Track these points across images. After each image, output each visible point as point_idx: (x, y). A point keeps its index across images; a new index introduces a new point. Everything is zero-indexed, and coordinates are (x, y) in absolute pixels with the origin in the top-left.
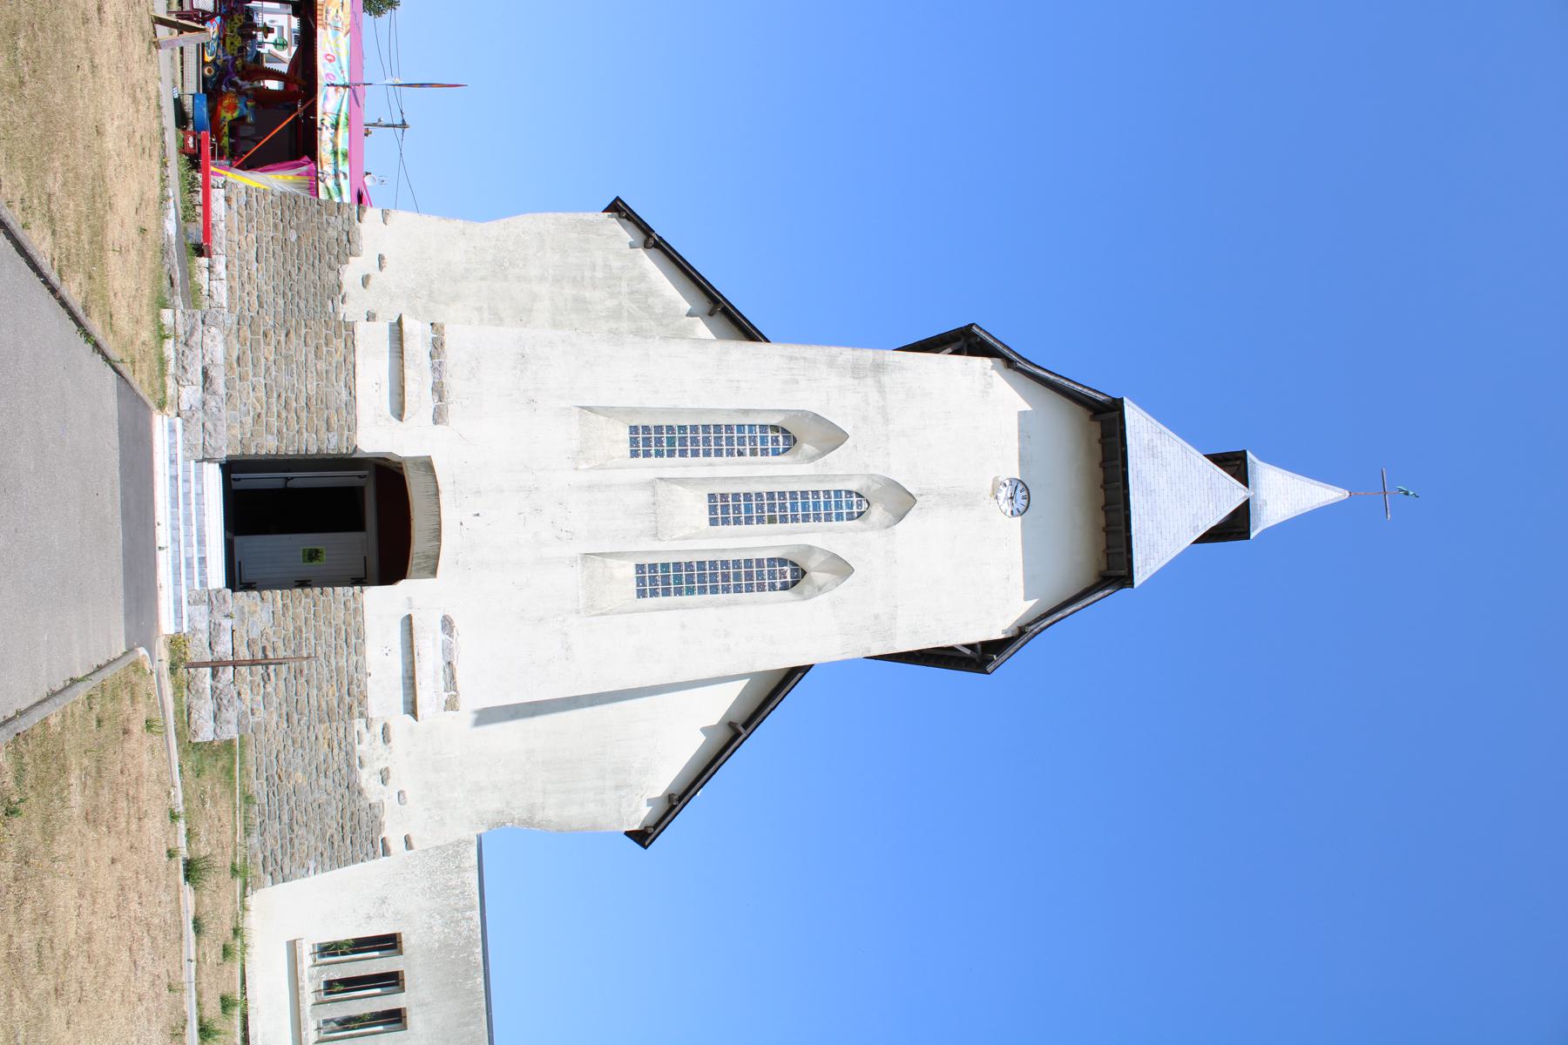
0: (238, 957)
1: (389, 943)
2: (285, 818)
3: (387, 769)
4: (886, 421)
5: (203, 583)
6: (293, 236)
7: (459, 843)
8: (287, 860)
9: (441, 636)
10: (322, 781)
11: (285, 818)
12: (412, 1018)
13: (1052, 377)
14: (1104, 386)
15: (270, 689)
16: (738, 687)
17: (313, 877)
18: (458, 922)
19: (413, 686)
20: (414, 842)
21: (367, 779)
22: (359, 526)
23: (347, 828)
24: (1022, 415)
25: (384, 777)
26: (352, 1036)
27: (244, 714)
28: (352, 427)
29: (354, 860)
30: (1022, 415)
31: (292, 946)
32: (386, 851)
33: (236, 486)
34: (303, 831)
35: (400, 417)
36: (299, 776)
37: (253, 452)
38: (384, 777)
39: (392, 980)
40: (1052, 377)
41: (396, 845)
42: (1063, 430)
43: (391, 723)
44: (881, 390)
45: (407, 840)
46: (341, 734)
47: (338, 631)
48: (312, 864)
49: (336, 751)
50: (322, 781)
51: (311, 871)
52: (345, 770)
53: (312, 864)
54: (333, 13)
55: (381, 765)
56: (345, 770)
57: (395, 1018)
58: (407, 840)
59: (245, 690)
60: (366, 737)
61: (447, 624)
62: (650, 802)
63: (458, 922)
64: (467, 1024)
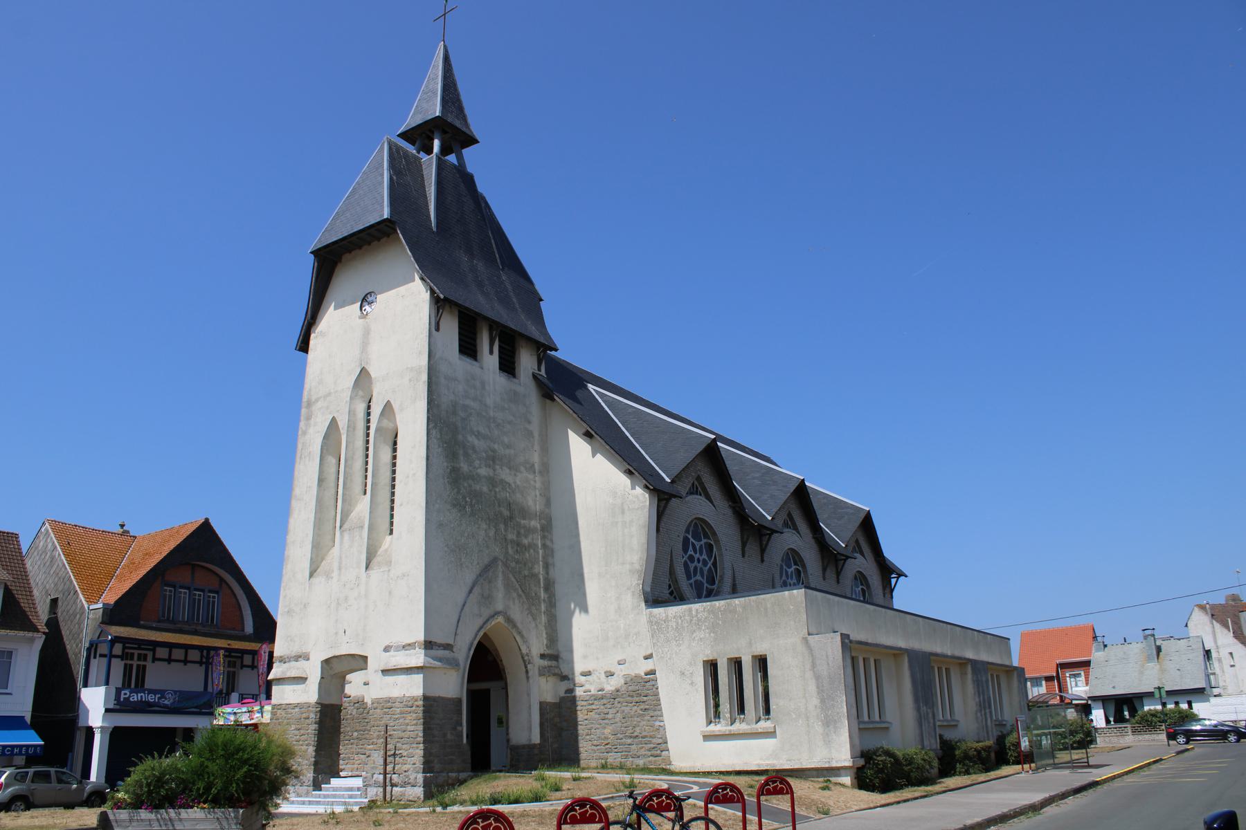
0: (731, 779)
1: (712, 667)
2: (629, 741)
4: (329, 394)
5: (359, 789)
6: (355, 734)
7: (650, 622)
8: (654, 740)
9: (392, 653)
11: (629, 741)
12: (760, 650)
14: (308, 265)
15: (405, 754)
16: (24, 551)
18: (699, 620)
19: (411, 669)
20: (649, 652)
21: (611, 685)
22: (487, 692)
23: (637, 699)
24: (335, 309)
25: (610, 674)
28: (308, 705)
29: (657, 695)
30: (335, 309)
31: (707, 738)
32: (653, 672)
34: (638, 729)
36: (607, 731)
38: (610, 674)
39: (737, 664)
42: (346, 281)
44: (317, 400)
45: (646, 658)
47: (385, 713)
48: (657, 723)
50: (610, 716)
52: (605, 701)
53: (657, 723)
54: (229, 710)
55: (603, 676)
57: (762, 663)
58: (646, 658)
59: (405, 767)
60: (587, 687)
61: (387, 649)
62: (633, 488)
63: (699, 620)
64: (766, 609)
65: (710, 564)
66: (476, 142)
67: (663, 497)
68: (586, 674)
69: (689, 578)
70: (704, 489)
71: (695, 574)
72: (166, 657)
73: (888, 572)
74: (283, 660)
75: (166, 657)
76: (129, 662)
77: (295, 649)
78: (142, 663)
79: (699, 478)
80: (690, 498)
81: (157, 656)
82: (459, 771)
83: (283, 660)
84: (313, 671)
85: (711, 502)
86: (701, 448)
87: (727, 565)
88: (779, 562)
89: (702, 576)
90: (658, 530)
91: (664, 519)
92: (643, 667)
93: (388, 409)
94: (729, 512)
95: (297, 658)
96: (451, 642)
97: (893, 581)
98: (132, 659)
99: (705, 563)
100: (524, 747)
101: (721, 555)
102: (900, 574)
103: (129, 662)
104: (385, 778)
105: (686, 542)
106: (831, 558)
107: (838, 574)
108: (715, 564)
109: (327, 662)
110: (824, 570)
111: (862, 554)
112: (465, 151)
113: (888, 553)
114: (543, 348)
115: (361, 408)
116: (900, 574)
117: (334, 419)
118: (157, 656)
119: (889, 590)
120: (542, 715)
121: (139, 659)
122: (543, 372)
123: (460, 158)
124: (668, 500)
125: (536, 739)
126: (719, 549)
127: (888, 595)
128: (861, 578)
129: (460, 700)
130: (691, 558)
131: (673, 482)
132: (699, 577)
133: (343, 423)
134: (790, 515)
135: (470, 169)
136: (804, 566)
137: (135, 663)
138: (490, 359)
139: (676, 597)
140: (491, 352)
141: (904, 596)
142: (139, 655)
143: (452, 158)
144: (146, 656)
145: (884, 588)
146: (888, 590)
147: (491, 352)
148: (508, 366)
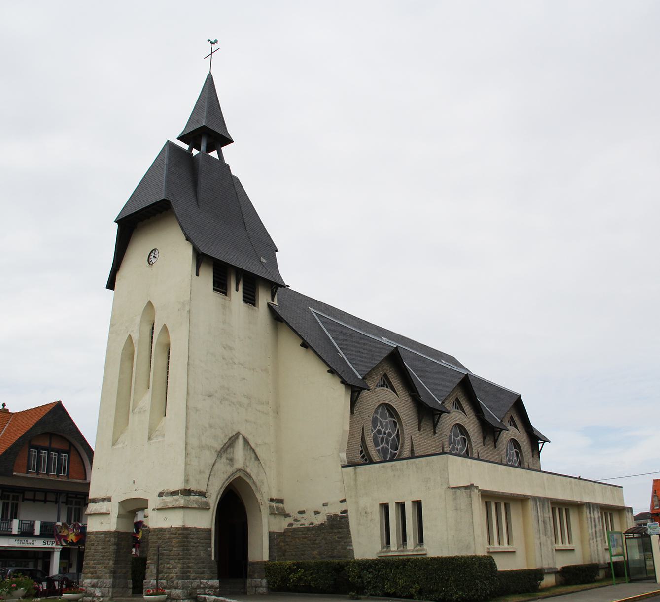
3: (315, 512)
10: (317, 542)
12: (416, 498)
13: (392, 342)
17: (354, 547)
25: (317, 513)
26: (213, 517)
27: (177, 576)
32: (346, 512)
33: (655, 580)
35: (109, 514)
36: (316, 552)
37: (217, 575)
39: (401, 506)
40: (392, 342)
41: (343, 507)
43: (298, 511)
46: (300, 533)
47: (159, 539)
48: (349, 548)
49: (307, 536)
50: (317, 542)
51: (351, 548)
52: (314, 532)
56: (314, 532)
57: (418, 505)
60: (302, 521)
65: (394, 435)
66: (232, 142)
67: (355, 391)
68: (152, 270)
69: (376, 445)
70: (390, 383)
71: (382, 443)
72: (43, 498)
73: (535, 439)
74: (94, 501)
75: (32, 498)
76: (6, 501)
77: (102, 495)
78: (15, 502)
79: (385, 375)
80: (378, 389)
81: (26, 497)
82: (208, 579)
83: (94, 501)
84: (114, 508)
85: (395, 392)
86: (385, 354)
87: (407, 436)
88: (448, 433)
89: (387, 443)
90: (352, 412)
91: (358, 405)
92: (336, 510)
93: (165, 328)
94: (409, 399)
95: (103, 500)
96: (204, 490)
97: (540, 445)
98: (8, 499)
99: (390, 435)
100: (258, 562)
101: (402, 429)
102: (545, 441)
103: (6, 501)
104: (157, 582)
105: (375, 422)
106: (490, 431)
107: (495, 441)
108: (398, 435)
109: (122, 503)
110: (484, 438)
111: (516, 426)
112: (223, 149)
113: (534, 422)
114: (275, 286)
115: (148, 329)
116: (545, 441)
117: (130, 336)
118: (26, 497)
119: (536, 451)
120: (270, 537)
121: (13, 499)
122: (275, 303)
123: (220, 154)
124: (359, 392)
125: (266, 558)
126: (401, 424)
127: (536, 456)
128: (515, 443)
129: (210, 530)
130: (379, 432)
131: (364, 378)
132: (384, 445)
133: (135, 337)
134: (457, 400)
135: (227, 161)
136: (468, 436)
137: (11, 502)
138: (236, 295)
139: (368, 460)
140: (237, 290)
141: (549, 458)
142: (13, 496)
143: (214, 154)
144: (18, 496)
145: (533, 451)
146: (535, 452)
147: (237, 290)
148: (250, 299)
